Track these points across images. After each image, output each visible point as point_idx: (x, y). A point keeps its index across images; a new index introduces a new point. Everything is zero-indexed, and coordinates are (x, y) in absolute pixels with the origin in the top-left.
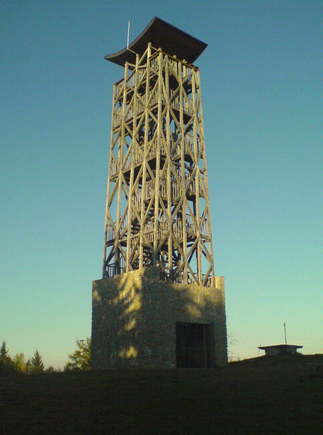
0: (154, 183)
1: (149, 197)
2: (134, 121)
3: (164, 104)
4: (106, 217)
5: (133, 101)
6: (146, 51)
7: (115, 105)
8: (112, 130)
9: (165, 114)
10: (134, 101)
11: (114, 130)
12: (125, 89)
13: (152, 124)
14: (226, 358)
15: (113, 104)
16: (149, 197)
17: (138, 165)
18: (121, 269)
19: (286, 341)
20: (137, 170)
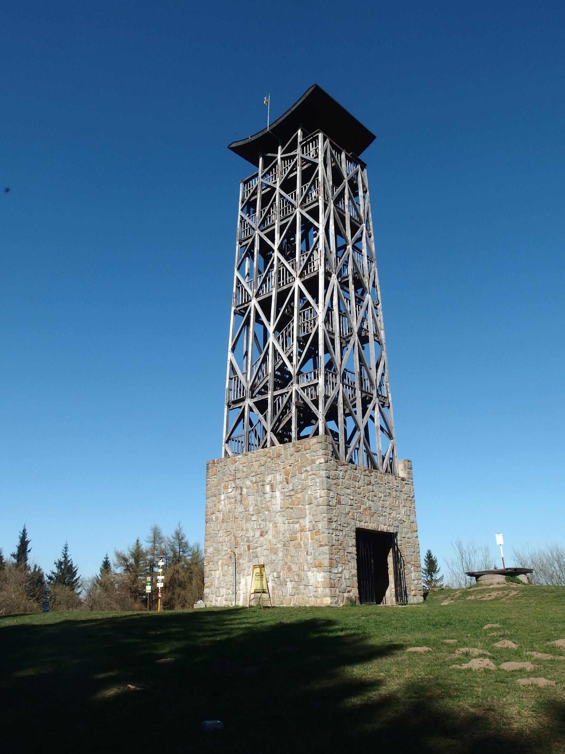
0: (307, 314)
1: (350, 331)
2: (276, 227)
3: (327, 202)
4: (384, 341)
5: (275, 200)
6: (317, 170)
7: (242, 210)
8: (238, 243)
9: (328, 215)
10: (292, 215)
11: (240, 243)
12: (259, 188)
13: (307, 227)
14: (496, 544)
15: (240, 208)
16: (350, 331)
17: (285, 288)
18: (159, 599)
19: (306, 92)
20: (282, 296)
